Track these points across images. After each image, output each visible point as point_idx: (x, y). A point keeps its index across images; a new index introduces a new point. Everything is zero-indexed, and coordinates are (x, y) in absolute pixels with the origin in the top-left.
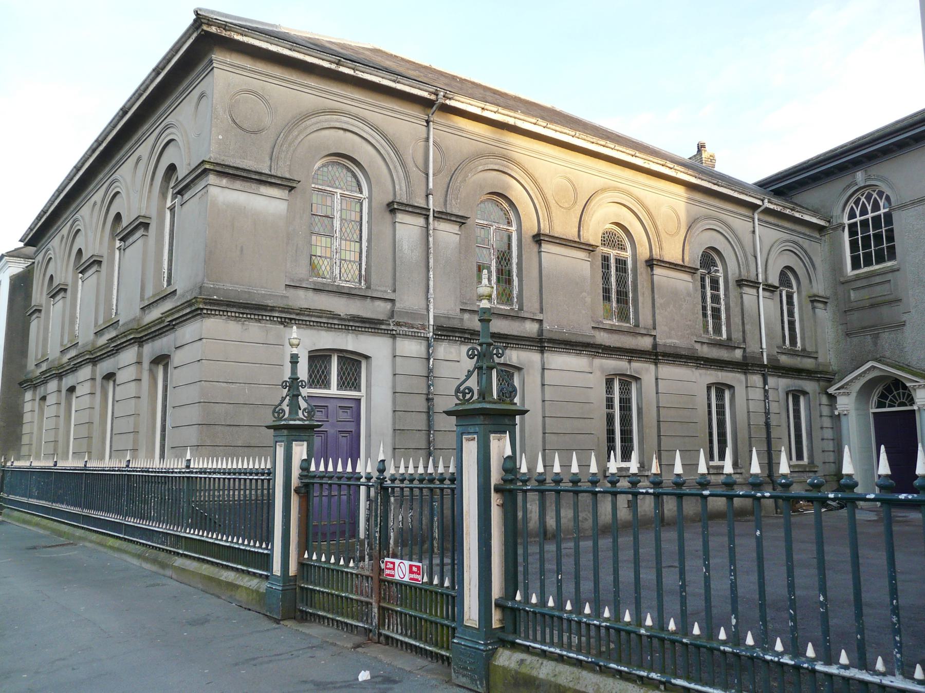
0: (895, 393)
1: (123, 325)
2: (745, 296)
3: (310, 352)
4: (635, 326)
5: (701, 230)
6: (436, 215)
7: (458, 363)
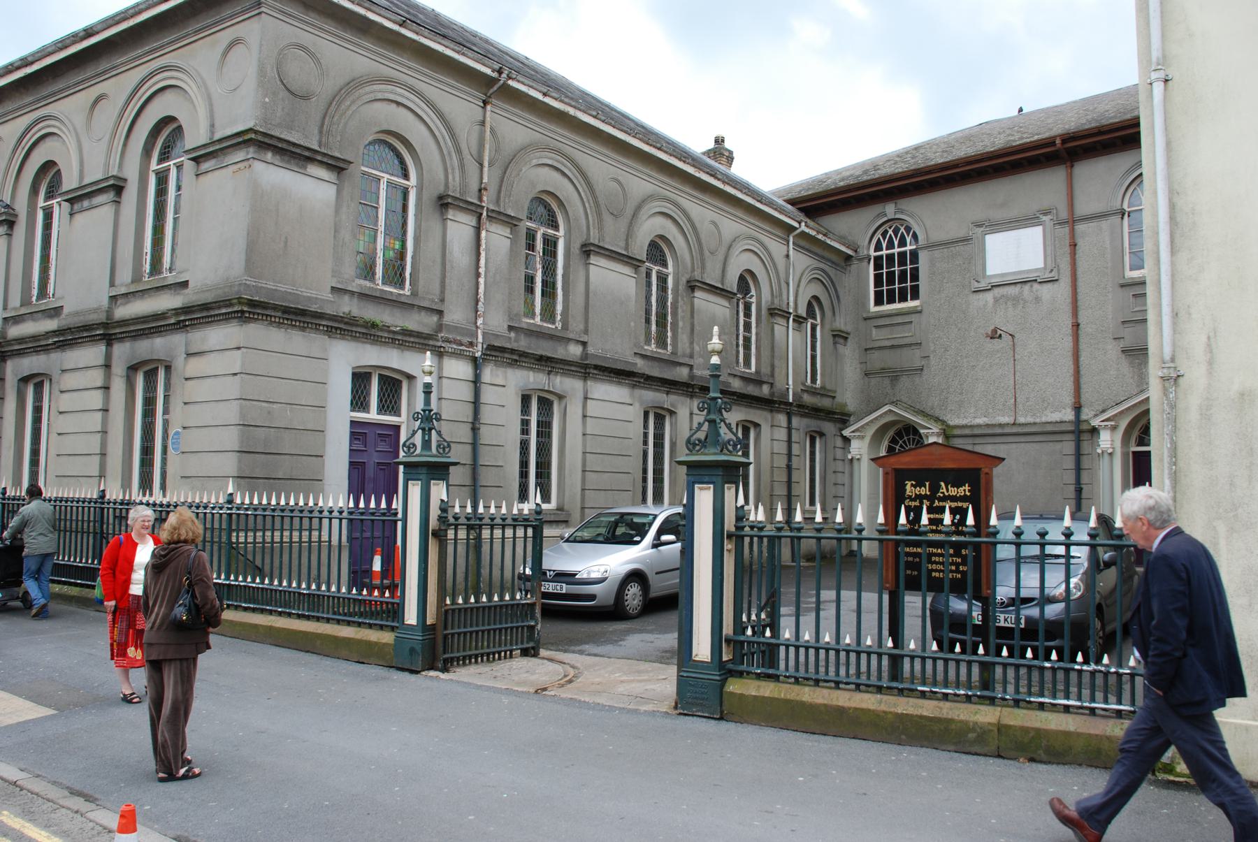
0: (905, 438)
1: (69, 315)
2: (776, 327)
3: (353, 368)
4: (672, 353)
5: (741, 250)
6: (490, 214)
7: (503, 388)
